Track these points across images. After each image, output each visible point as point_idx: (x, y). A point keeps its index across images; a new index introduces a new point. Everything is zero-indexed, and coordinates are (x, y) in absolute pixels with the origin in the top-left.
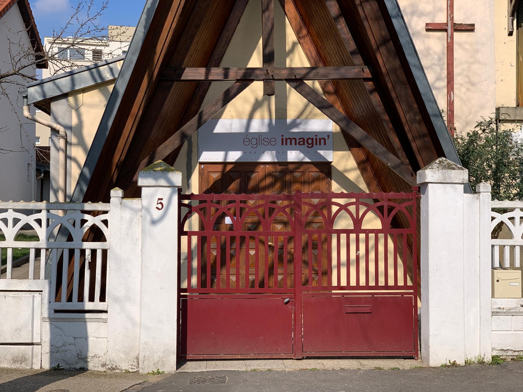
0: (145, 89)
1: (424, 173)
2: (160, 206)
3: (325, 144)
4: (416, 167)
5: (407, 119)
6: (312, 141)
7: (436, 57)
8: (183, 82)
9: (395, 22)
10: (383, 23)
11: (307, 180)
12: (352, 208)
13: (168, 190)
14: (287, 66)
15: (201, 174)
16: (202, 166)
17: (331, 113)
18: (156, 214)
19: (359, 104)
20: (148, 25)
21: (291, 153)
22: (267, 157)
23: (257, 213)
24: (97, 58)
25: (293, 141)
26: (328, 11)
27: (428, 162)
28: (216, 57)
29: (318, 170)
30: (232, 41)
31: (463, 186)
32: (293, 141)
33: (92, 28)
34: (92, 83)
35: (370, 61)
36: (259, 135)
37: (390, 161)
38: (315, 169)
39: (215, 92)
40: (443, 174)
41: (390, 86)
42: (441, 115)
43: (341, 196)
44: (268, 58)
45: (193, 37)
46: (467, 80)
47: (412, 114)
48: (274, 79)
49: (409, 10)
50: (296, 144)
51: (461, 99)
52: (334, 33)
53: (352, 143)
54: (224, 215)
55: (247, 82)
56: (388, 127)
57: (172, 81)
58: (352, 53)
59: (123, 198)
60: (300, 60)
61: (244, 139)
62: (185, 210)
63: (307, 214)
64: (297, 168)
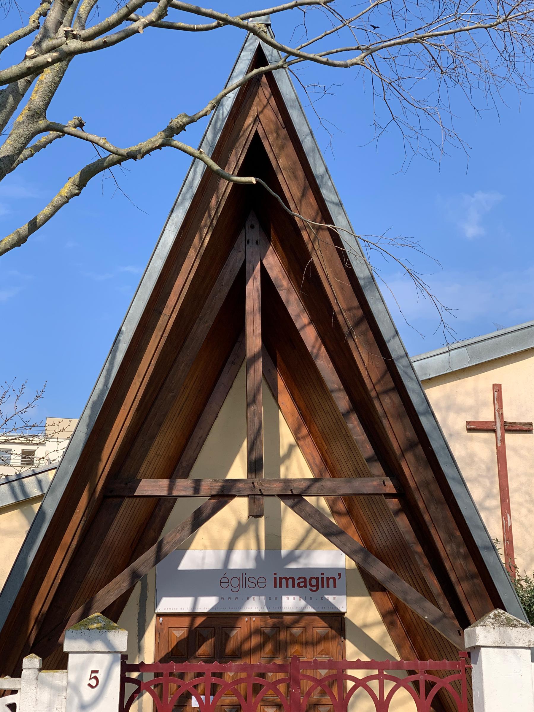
0: (83, 510)
1: (474, 632)
2: (93, 682)
3: (335, 586)
4: (465, 622)
5: (448, 552)
6: (315, 582)
7: (484, 466)
8: (138, 499)
9: (424, 421)
10: (407, 421)
11: (310, 639)
12: (374, 684)
13: (107, 658)
14: (282, 477)
15: (158, 631)
16: (161, 619)
17: (341, 542)
18: (88, 694)
19: (381, 528)
20: (93, 423)
21: (287, 599)
22: (254, 605)
23: (236, 693)
24: (27, 461)
25: (290, 581)
26: (335, 404)
27: (481, 615)
28: (184, 464)
29: (326, 625)
30: (207, 443)
31: (529, 651)
32: (290, 581)
33: (20, 424)
34: (11, 501)
35: (393, 470)
36: (243, 572)
37: (428, 612)
38: (322, 623)
39: (182, 512)
40: (500, 634)
41: (421, 505)
42: (494, 547)
43: (358, 665)
44: (255, 466)
45: (152, 438)
46: (527, 497)
47: (453, 545)
48: (262, 495)
49: (443, 404)
50: (294, 586)
51: (522, 524)
52: (344, 433)
53: (373, 586)
54: (187, 697)
55: (226, 499)
56: (422, 562)
57: (123, 497)
58: (369, 460)
59: (40, 670)
60: (298, 468)
61: (222, 579)
62: (131, 688)
63: (309, 694)
64: (297, 622)
